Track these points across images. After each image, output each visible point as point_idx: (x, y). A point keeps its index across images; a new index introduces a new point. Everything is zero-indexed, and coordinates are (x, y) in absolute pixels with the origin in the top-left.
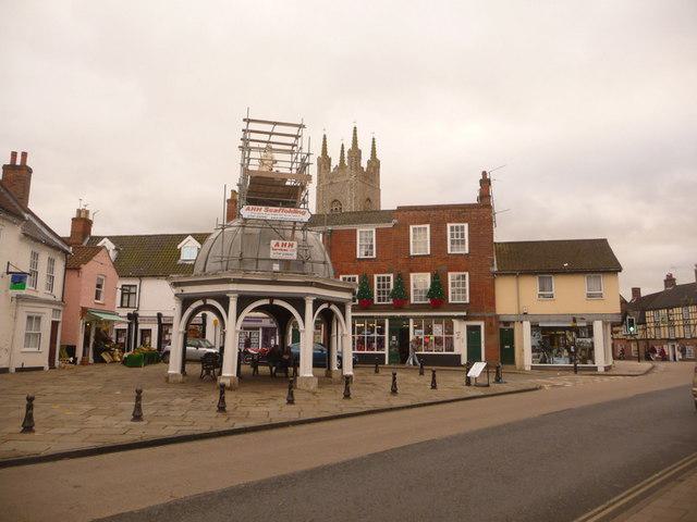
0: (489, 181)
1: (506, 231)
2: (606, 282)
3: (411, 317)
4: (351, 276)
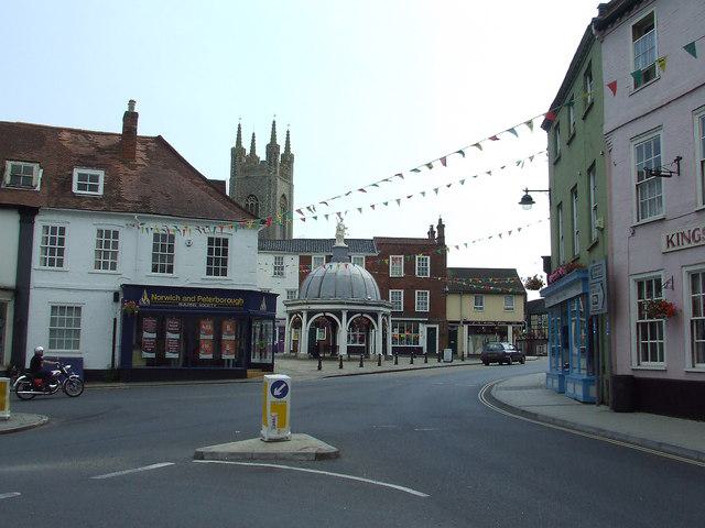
0: (292, 157)
1: (454, 260)
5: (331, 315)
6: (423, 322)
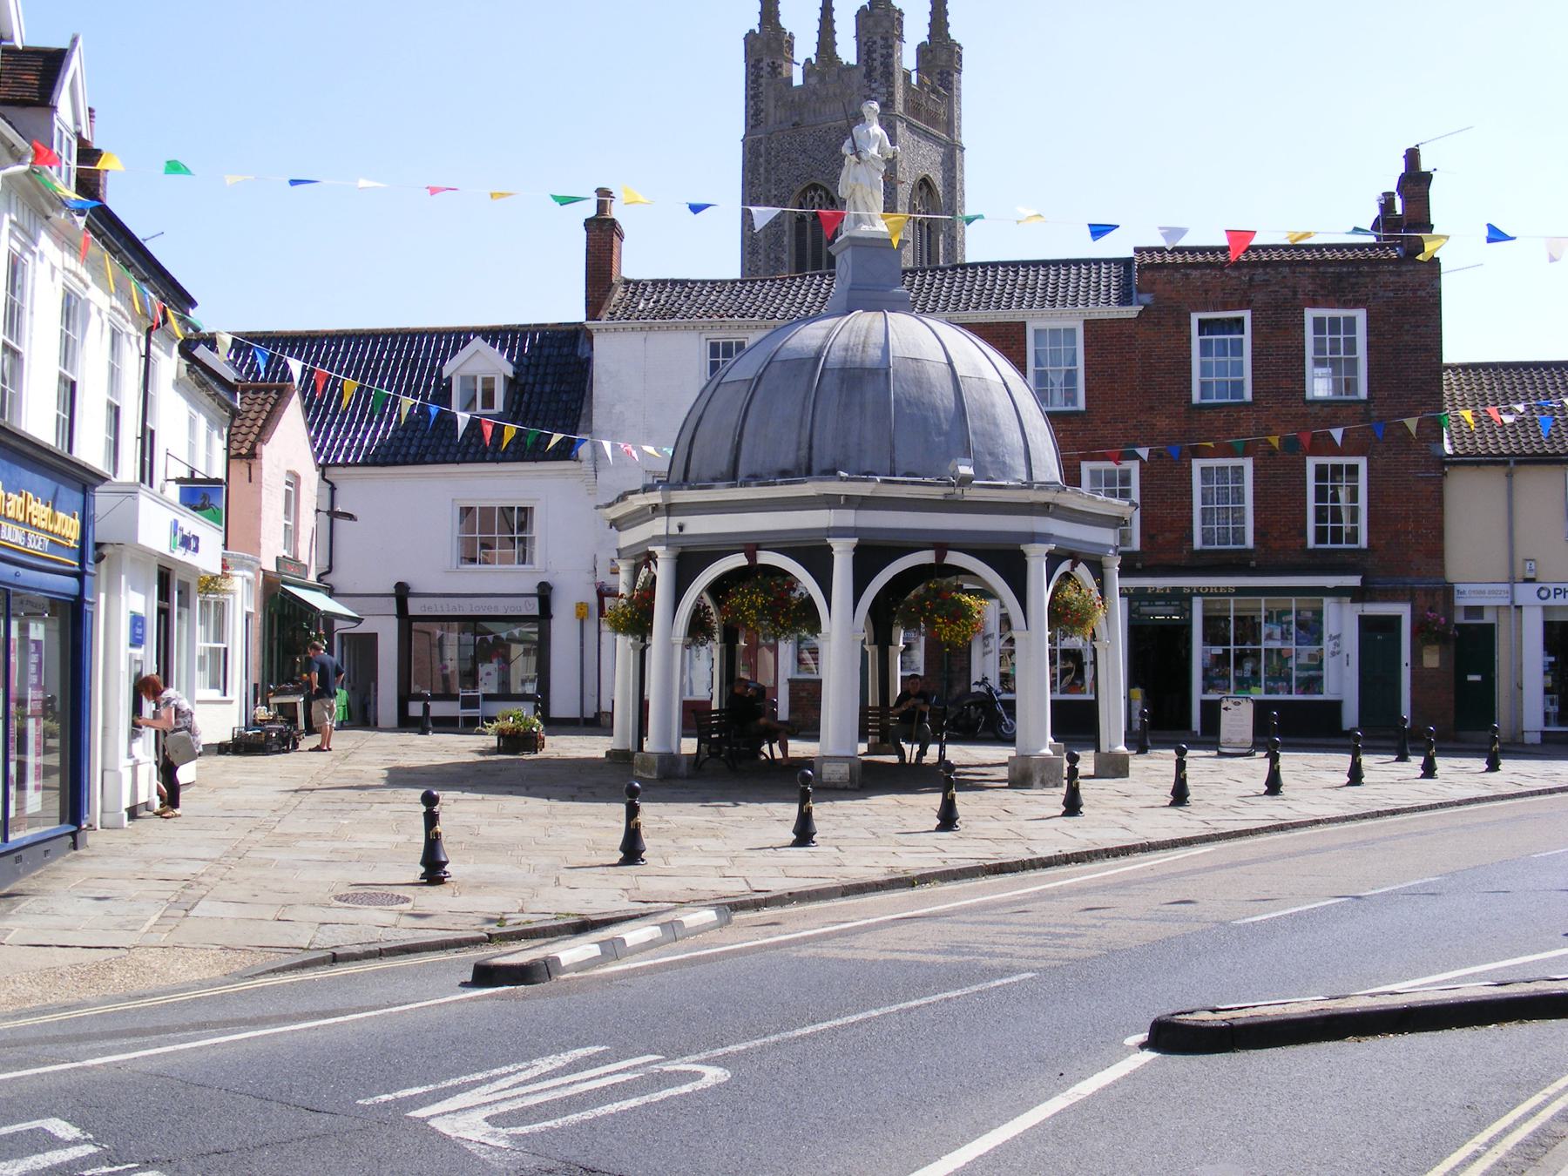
3: (1199, 592)
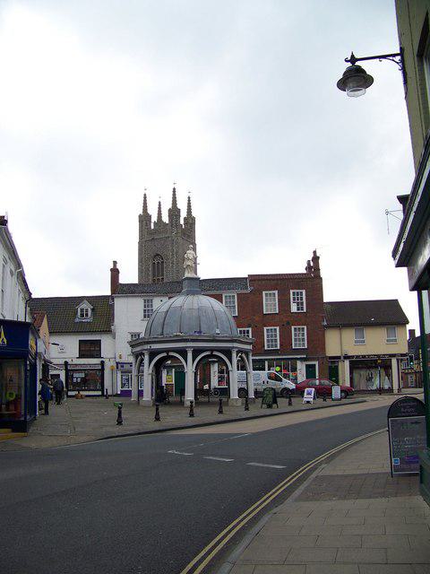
0: (194, 219)
1: (331, 294)
2: (398, 330)
4: (246, 329)
5: (177, 356)
6: (301, 359)
